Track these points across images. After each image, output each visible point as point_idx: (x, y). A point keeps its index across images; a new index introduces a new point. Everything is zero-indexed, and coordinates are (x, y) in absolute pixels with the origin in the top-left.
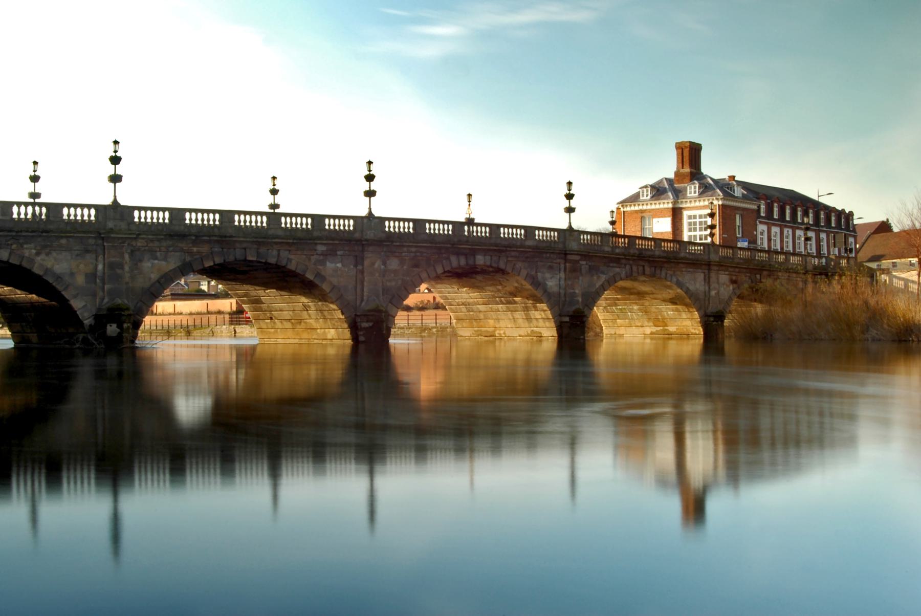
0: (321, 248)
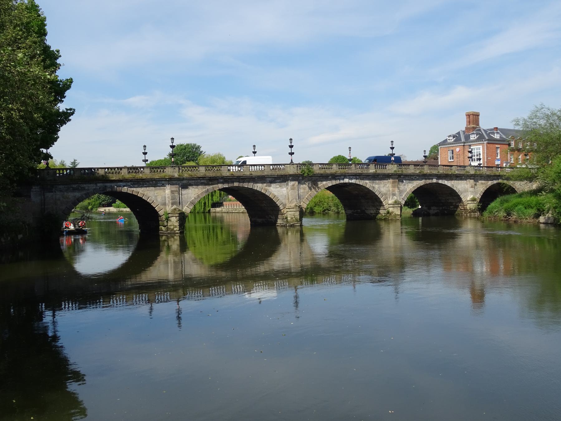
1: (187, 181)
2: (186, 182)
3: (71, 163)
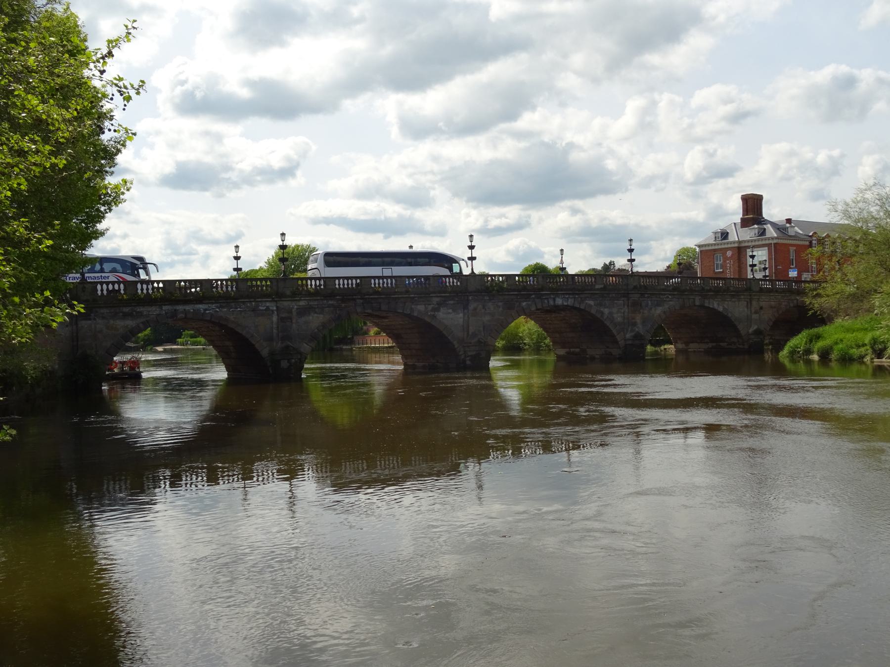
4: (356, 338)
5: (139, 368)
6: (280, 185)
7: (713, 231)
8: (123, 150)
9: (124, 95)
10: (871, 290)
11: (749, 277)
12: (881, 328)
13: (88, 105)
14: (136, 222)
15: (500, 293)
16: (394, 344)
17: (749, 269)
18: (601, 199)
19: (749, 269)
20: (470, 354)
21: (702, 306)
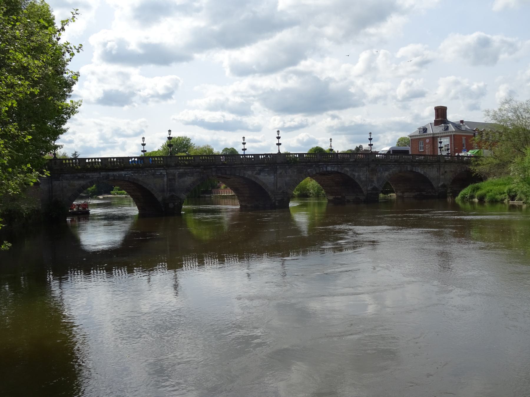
0: (258, 168)
1: (183, 169)
2: (182, 171)
3: (72, 155)
4: (213, 191)
5: (88, 208)
6: (163, 103)
7: (418, 128)
8: (76, 82)
9: (70, 53)
10: (508, 162)
11: (439, 154)
12: (514, 183)
13: (50, 58)
14: (81, 125)
15: (295, 164)
16: (235, 194)
17: (439, 149)
18: (350, 110)
19: (439, 149)
20: (278, 199)
21: (411, 171)
